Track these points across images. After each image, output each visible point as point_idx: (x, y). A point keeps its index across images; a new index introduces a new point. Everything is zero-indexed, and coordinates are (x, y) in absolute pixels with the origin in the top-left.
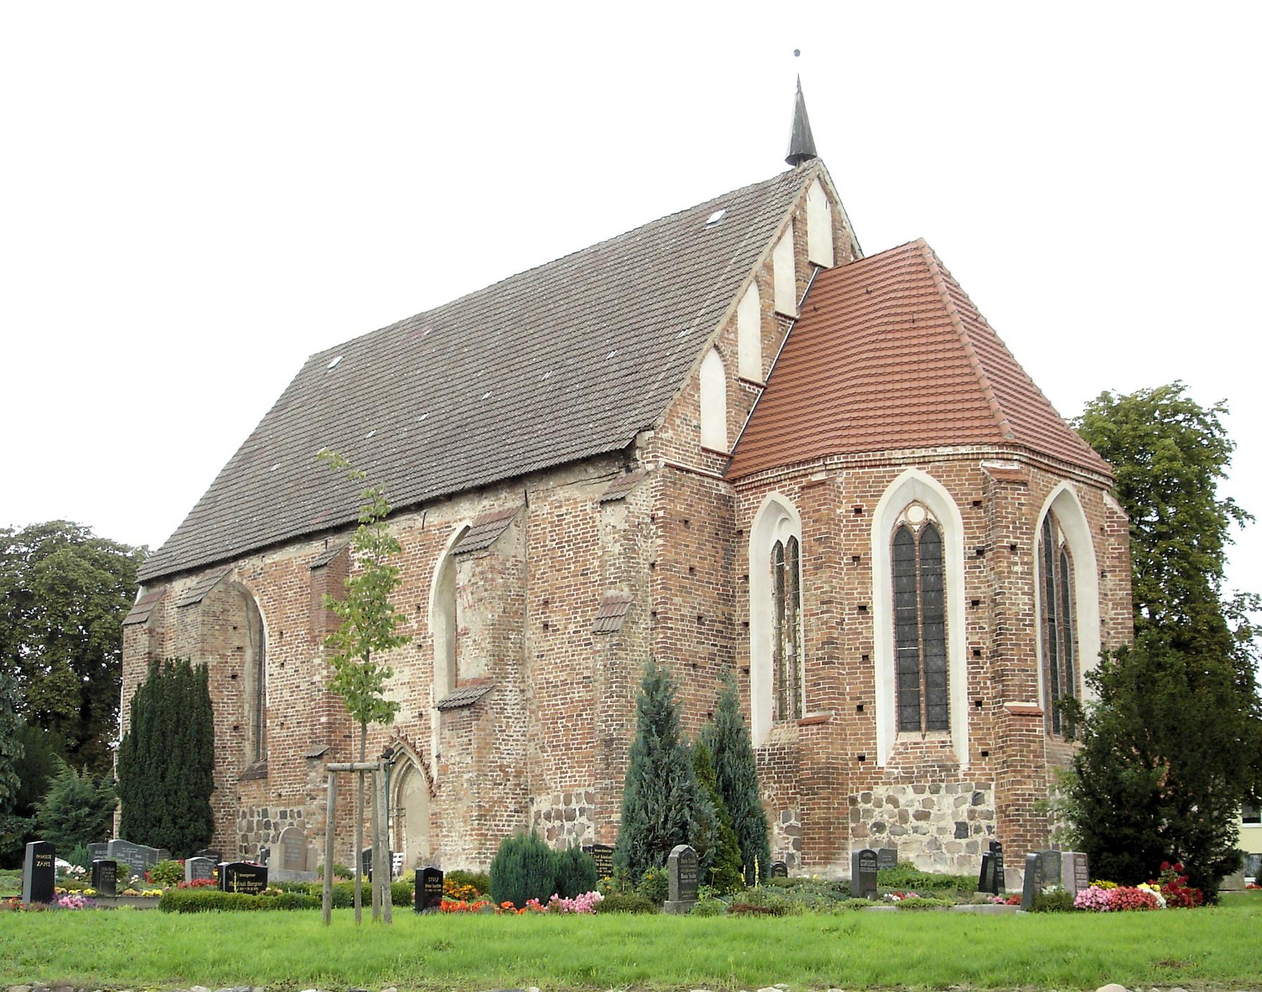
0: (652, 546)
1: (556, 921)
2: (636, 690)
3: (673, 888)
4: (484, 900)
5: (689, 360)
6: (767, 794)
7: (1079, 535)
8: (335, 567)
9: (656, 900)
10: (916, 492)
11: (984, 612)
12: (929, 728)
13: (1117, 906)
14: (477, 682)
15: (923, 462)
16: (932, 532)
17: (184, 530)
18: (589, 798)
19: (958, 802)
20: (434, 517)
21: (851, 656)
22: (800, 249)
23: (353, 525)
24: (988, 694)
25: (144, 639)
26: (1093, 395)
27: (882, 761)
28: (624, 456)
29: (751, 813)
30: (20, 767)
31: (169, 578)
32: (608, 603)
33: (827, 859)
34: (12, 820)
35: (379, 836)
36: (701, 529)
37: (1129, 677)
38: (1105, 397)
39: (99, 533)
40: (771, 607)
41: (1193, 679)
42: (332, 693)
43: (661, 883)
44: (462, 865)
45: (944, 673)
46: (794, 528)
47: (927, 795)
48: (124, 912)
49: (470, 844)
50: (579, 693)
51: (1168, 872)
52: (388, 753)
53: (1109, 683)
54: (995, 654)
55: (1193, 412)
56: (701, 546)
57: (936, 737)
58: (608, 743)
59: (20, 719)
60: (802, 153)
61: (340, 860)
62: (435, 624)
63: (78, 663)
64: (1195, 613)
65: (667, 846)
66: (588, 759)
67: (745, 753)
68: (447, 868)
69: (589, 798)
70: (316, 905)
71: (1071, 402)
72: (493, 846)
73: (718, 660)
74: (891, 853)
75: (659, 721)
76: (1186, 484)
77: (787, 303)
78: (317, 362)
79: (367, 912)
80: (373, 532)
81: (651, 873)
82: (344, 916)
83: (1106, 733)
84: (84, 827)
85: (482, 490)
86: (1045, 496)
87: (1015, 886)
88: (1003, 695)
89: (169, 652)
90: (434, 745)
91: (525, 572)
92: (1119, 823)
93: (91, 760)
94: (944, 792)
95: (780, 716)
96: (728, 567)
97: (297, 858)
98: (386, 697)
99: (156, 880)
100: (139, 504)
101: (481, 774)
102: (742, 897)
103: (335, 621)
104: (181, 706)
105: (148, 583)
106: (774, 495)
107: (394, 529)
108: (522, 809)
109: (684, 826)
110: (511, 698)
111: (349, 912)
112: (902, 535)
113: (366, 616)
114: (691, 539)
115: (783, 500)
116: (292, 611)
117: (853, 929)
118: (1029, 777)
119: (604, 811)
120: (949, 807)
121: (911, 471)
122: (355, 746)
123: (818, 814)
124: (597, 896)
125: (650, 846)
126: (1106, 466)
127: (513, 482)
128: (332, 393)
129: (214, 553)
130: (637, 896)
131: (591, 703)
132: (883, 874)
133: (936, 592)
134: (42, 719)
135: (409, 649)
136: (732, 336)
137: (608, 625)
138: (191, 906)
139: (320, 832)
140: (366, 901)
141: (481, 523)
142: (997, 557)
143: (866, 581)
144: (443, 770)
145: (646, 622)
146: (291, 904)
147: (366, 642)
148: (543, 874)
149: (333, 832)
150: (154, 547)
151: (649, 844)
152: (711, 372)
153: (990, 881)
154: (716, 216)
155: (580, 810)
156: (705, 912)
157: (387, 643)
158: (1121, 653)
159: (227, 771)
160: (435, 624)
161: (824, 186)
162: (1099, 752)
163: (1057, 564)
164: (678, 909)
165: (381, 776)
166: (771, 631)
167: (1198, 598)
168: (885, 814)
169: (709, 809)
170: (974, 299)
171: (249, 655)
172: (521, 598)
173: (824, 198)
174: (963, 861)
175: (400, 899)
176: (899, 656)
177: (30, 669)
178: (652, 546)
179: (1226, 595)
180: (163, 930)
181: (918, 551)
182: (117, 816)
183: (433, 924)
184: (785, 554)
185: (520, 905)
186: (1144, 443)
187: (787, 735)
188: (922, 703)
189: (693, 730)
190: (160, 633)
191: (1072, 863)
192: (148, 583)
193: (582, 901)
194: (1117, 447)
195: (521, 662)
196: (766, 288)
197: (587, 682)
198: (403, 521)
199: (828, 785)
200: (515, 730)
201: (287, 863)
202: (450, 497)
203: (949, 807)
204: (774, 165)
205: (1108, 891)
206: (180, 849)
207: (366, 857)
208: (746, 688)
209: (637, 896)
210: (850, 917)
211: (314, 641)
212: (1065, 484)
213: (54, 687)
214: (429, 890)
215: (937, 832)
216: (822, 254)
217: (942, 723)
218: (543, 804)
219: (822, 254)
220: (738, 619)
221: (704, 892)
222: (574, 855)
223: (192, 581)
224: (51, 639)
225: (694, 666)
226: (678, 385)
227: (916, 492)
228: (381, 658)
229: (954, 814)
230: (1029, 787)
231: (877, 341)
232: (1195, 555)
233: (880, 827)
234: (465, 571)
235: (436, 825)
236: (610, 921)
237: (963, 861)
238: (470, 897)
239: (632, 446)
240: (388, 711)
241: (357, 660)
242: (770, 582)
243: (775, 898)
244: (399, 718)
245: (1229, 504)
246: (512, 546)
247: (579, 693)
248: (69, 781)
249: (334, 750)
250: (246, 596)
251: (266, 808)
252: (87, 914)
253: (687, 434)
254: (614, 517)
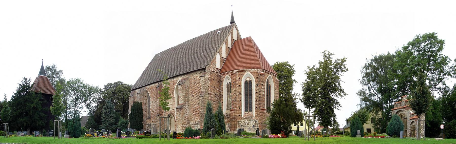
0: (209, 83)
1: (194, 140)
2: (206, 105)
3: (211, 135)
4: (183, 137)
5: (214, 54)
6: (225, 121)
7: (272, 83)
8: (160, 87)
9: (209, 137)
10: (248, 76)
11: (258, 94)
13: (274, 138)
14: (182, 104)
15: (249, 71)
16: (250, 82)
17: (137, 82)
18: (199, 122)
19: (253, 122)
20: (175, 79)
21: (238, 100)
22: (232, 37)
23: (163, 80)
24: (258, 106)
25: (132, 99)
26: (275, 62)
27: (242, 116)
28: (204, 69)
29: (223, 124)
30: (115, 118)
31: (135, 89)
32: (202, 92)
33: (234, 130)
34: (114, 126)
35: (167, 127)
37: (278, 104)
38: (277, 62)
39: (125, 83)
40: (226, 93)
41: (287, 106)
42: (160, 106)
43: (210, 134)
44: (180, 132)
45: (252, 103)
46: (230, 81)
48: (131, 138)
49: (181, 129)
50: (197, 106)
51: (282, 133)
52: (169, 115)
53: (275, 106)
54: (259, 100)
55: (290, 66)
57: (250, 112)
58: (202, 113)
59: (115, 111)
60: (232, 22)
61: (162, 131)
62: (175, 96)
63: (123, 103)
64: (288, 96)
65: (211, 129)
66: (199, 116)
67: (222, 115)
68: (177, 132)
69: (199, 122)
70: (158, 138)
71: (272, 63)
72: (184, 129)
74: (243, 130)
75: (209, 110)
76: (288, 77)
77: (230, 45)
78: (157, 55)
79: (166, 139)
80: (166, 82)
81: (208, 133)
82: (163, 139)
83: (274, 112)
84: (124, 126)
85: (182, 75)
87: (261, 135)
88: (260, 106)
89: (136, 100)
90: (175, 114)
91: (189, 87)
92: (275, 126)
93: (125, 117)
94: (250, 120)
95: (228, 109)
96: (220, 86)
97: (155, 131)
98: (168, 107)
99: (135, 134)
100: (131, 79)
101: (182, 118)
102: (221, 136)
103: (160, 95)
104: (138, 108)
105: (132, 90)
106: (227, 76)
107: (169, 81)
108: (189, 123)
109: (213, 126)
110: (187, 106)
111: (163, 139)
112: (246, 82)
113: (165, 95)
114: (214, 82)
115: (229, 76)
116: (154, 94)
117: (237, 141)
119: (201, 124)
120: (252, 123)
121: (248, 72)
122: (164, 114)
123: (233, 124)
124: (200, 136)
125: (208, 129)
126: (276, 73)
127: (187, 73)
128: (159, 60)
129: (142, 84)
130: (206, 136)
131: (199, 107)
132: (242, 133)
133: (251, 91)
134: (118, 111)
135: (171, 99)
137: (202, 95)
138: (141, 138)
139: (159, 127)
140: (166, 137)
141: (182, 80)
142: (260, 86)
143: (241, 89)
144: (177, 118)
145: (207, 95)
146: (155, 137)
147: (165, 98)
148: (192, 133)
149: (161, 127)
150: (133, 85)
151: (207, 128)
152: (218, 57)
153: (257, 134)
154: (219, 32)
155: (197, 123)
156: (216, 138)
157: (168, 98)
158: (276, 101)
159: (145, 118)
160: (175, 96)
161: (236, 27)
162: (273, 115)
163: (268, 87)
164: (212, 138)
165: (168, 118)
166: (226, 96)
167: (289, 93)
168: (243, 124)
169: (217, 123)
170: (258, 46)
171: (147, 101)
172: (188, 91)
174: (254, 131)
175: (171, 137)
176: (245, 100)
177: (116, 104)
178: (209, 83)
179: (293, 93)
180: (137, 141)
181: (248, 84)
182: (129, 125)
183: (176, 140)
184: (229, 85)
185: (188, 138)
186: (283, 70)
187: (229, 112)
188: (248, 107)
189: (214, 111)
190: (135, 97)
191: (269, 131)
192: (132, 90)
193: (198, 137)
194: (278, 70)
195: (188, 101)
196: (227, 43)
197: (198, 104)
198: (170, 80)
199: (235, 119)
200: (187, 111)
201: (154, 132)
202: (177, 76)
203: (252, 123)
204: (228, 24)
205: (273, 135)
206: (139, 129)
207: (166, 130)
208: (223, 105)
209: (206, 136)
210: (237, 139)
211: (157, 98)
212: (270, 75)
213: (119, 106)
214: (175, 135)
215: (250, 126)
216: (235, 38)
217: (251, 111)
218: (192, 123)
219: (235, 38)
220: (222, 94)
221: (216, 136)
222: (196, 130)
223: (139, 90)
224: (118, 99)
226: (213, 59)
227: (248, 76)
228: (167, 101)
230: (263, 120)
231: (243, 52)
232: (289, 87)
233: (242, 126)
234: (180, 88)
235: (176, 126)
236: (202, 140)
237: (254, 131)
238: (181, 136)
239: (205, 68)
240: (168, 109)
241: (164, 101)
242: (226, 89)
243: (226, 136)
244: (170, 110)
245: (294, 80)
246: (187, 83)
247: (197, 106)
248: (122, 120)
249: (160, 115)
250: (147, 92)
251: (151, 123)
252: (126, 139)
253: (214, 66)
254: (203, 79)
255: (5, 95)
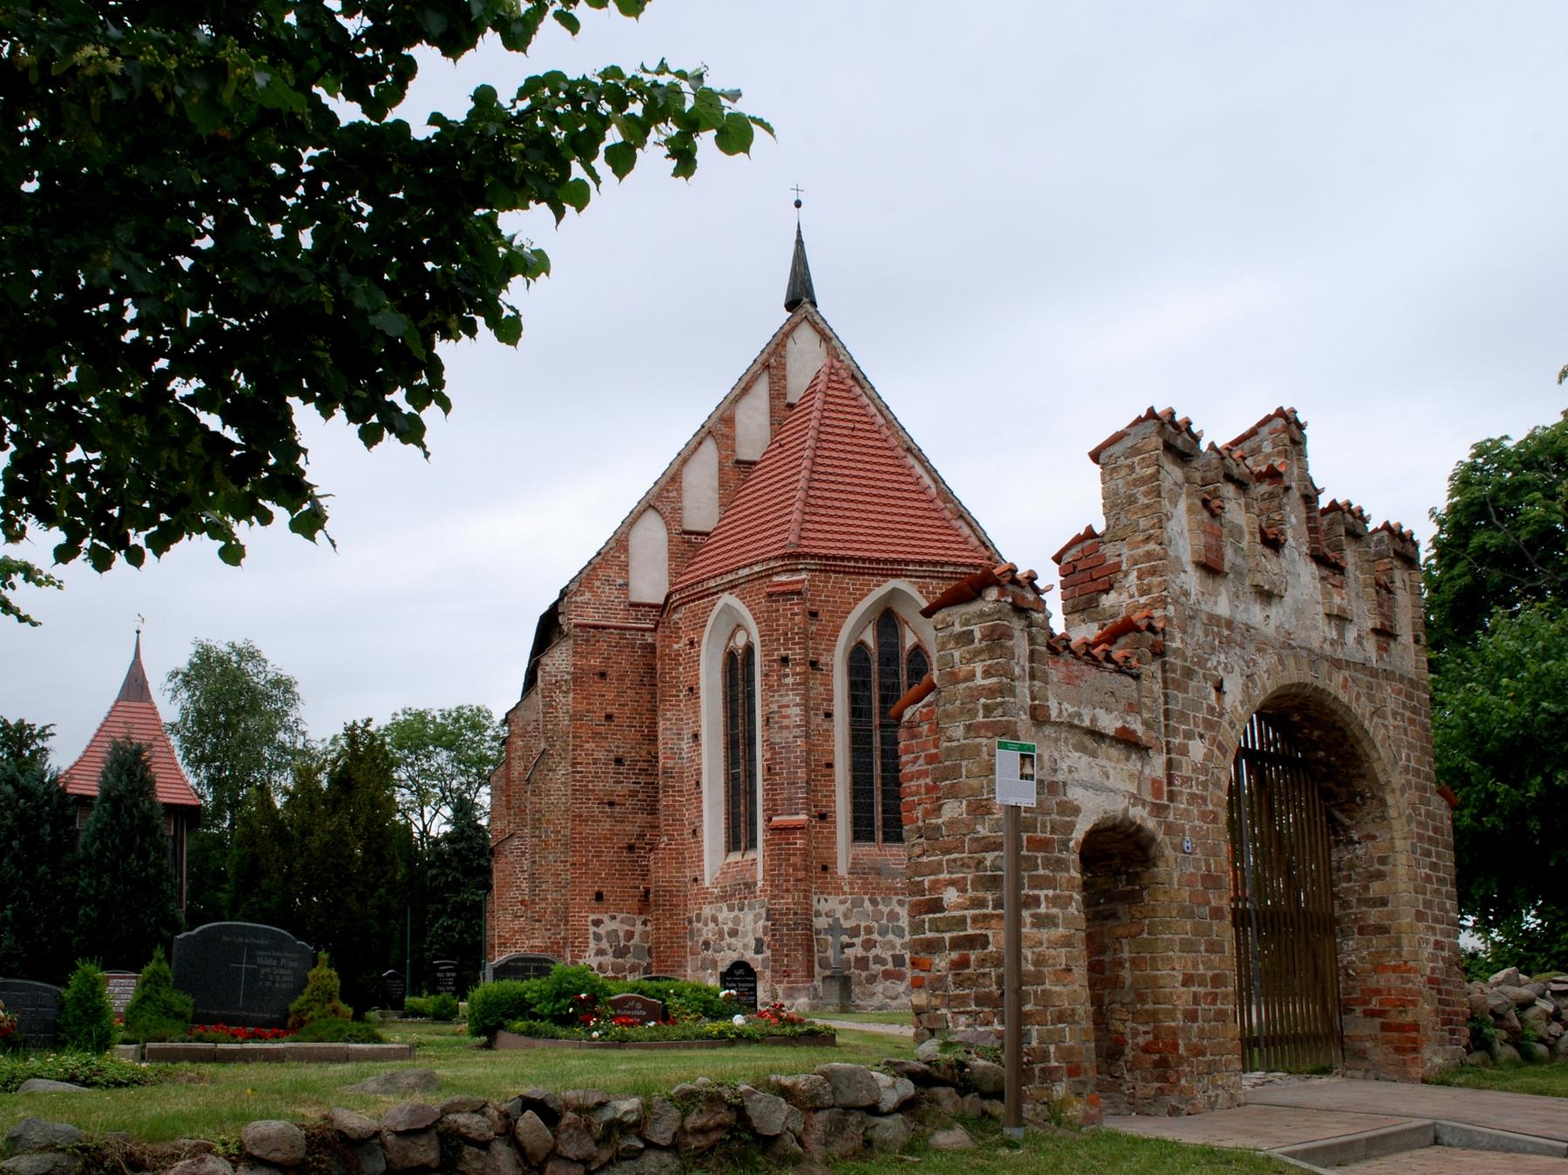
12: (885, 840)
15: (732, 587)
19: (756, 919)
27: (707, 884)
36: (621, 678)
47: (736, 912)
56: (620, 694)
60: (800, 296)
73: (640, 796)
86: (857, 601)
118: (787, 891)
136: (674, 494)
168: (708, 932)
173: (816, 338)
181: (737, 668)
225: (611, 804)
229: (754, 930)
255: (34, 624)
